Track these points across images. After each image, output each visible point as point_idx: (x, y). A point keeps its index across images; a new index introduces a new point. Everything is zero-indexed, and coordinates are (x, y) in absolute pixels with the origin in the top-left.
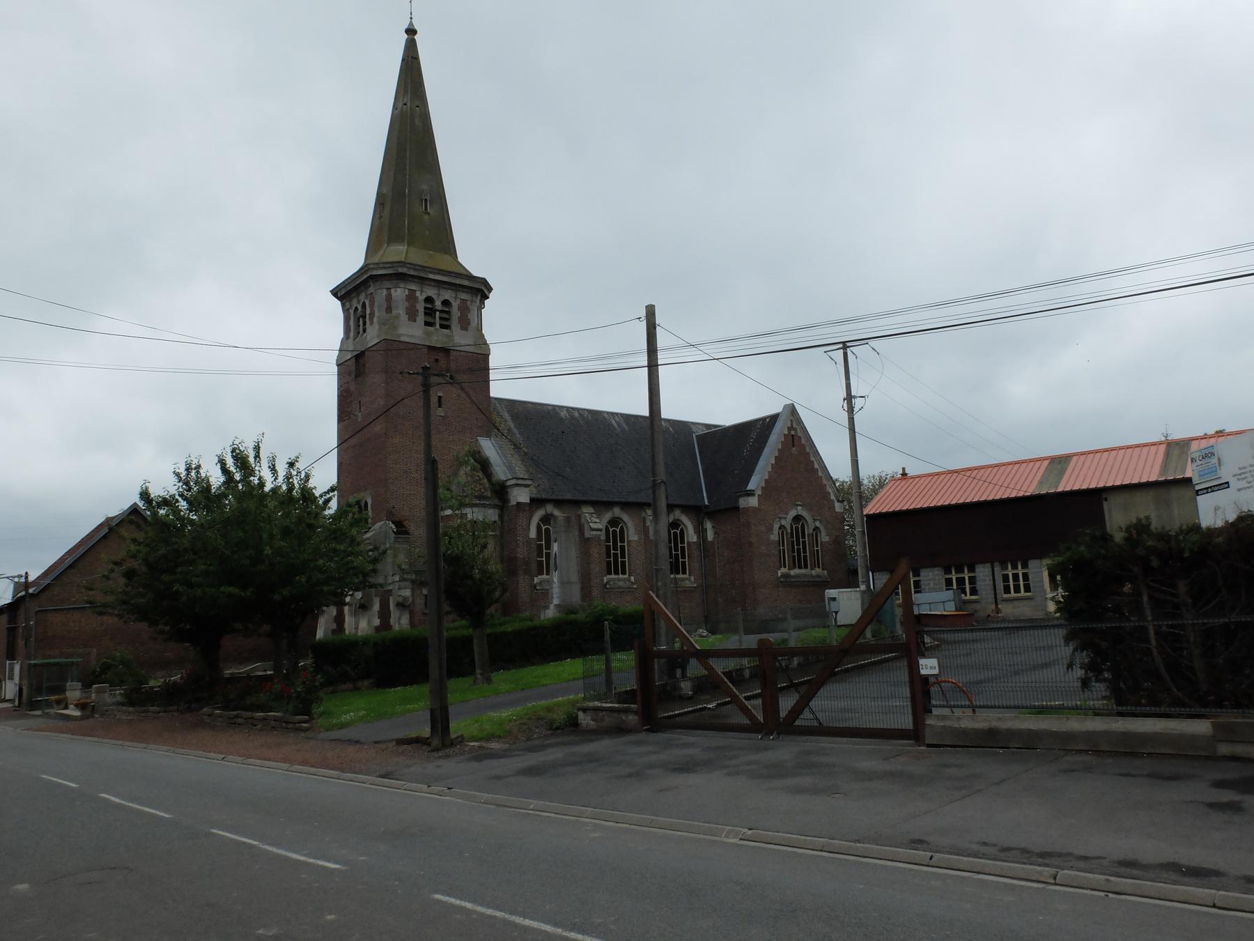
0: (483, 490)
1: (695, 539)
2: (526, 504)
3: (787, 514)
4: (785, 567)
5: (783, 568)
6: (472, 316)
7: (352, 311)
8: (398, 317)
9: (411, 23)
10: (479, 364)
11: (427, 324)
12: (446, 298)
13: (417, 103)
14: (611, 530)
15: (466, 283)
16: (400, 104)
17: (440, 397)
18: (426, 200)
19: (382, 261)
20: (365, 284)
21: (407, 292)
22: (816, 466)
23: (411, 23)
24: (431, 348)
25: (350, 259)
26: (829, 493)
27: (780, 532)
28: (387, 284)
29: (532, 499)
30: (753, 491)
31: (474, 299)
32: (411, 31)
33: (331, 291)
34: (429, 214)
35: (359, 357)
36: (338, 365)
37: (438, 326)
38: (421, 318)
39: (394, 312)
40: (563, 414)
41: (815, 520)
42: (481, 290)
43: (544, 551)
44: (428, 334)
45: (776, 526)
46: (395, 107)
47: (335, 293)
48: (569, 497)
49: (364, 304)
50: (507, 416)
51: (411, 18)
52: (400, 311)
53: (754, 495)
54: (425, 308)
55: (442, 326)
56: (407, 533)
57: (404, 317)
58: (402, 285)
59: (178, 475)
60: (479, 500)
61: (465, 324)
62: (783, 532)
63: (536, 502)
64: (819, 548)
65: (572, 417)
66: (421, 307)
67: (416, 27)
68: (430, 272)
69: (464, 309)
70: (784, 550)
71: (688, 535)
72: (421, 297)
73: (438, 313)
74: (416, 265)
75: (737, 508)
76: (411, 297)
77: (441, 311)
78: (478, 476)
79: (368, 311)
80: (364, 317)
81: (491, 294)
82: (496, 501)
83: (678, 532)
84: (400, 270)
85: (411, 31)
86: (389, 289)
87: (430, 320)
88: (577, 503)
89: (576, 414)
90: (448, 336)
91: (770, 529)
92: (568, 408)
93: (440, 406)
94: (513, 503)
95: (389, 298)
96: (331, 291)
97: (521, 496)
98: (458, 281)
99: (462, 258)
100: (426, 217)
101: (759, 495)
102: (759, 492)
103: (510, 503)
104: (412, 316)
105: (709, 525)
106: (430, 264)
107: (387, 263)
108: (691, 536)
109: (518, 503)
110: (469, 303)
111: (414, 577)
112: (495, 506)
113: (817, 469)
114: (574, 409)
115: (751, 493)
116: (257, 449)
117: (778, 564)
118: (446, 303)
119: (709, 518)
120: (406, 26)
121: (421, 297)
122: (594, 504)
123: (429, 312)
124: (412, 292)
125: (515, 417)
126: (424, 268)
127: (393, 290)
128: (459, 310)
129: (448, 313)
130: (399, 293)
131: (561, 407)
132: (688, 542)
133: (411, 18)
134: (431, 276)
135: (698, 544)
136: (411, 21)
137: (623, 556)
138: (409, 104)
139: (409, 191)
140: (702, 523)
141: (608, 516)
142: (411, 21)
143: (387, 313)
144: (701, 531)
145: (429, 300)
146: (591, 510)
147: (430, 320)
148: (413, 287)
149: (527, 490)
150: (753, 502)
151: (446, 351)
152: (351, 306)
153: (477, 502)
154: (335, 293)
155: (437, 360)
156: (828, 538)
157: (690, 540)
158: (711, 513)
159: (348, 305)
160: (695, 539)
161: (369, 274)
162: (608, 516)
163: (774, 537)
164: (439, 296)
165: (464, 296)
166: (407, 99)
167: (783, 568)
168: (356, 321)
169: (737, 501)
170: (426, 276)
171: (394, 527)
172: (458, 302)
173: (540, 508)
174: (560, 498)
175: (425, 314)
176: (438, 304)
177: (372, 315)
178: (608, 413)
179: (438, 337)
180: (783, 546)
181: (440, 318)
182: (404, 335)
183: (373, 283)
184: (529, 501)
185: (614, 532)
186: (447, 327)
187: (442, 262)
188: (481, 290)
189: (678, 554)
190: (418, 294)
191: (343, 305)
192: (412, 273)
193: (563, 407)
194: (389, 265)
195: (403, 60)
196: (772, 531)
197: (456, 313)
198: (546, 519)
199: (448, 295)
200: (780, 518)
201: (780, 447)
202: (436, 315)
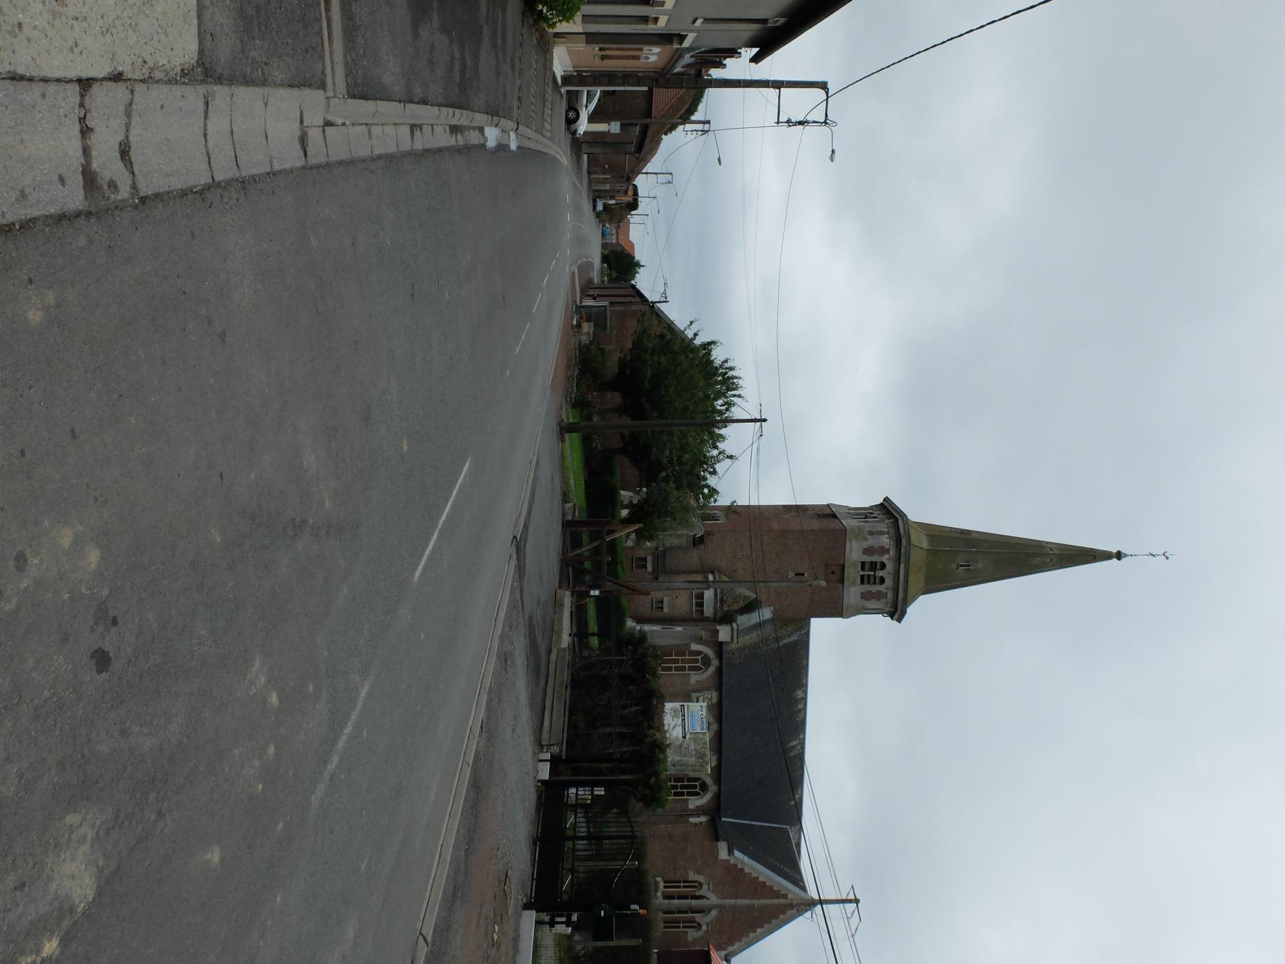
0: (728, 603)
1: (691, 806)
2: (718, 638)
3: (712, 891)
4: (665, 887)
5: (663, 925)
6: (872, 604)
7: (871, 511)
8: (865, 539)
9: (1126, 555)
10: (836, 609)
11: (863, 564)
12: (886, 581)
13: (1054, 560)
14: (697, 783)
15: (901, 596)
16: (1051, 546)
17: (803, 575)
18: (969, 566)
19: (910, 528)
20: (893, 516)
21: (887, 547)
22: (759, 930)
23: (1126, 555)
24: (843, 566)
25: (917, 511)
26: (733, 945)
27: (696, 884)
28: (892, 531)
29: (721, 642)
30: (733, 854)
31: (889, 605)
32: (1119, 556)
33: (887, 497)
34: (958, 568)
35: (834, 516)
36: (828, 505)
37: (862, 573)
38: (868, 559)
39: (869, 537)
40: (799, 693)
41: (708, 924)
42: (896, 612)
43: (679, 784)
44: (854, 564)
45: (701, 878)
46: (1048, 543)
47: (886, 499)
48: (725, 680)
49: (876, 518)
50: (794, 638)
51: (1131, 555)
52: (871, 541)
53: (729, 855)
54: (876, 562)
55: (862, 577)
56: (694, 546)
57: (866, 545)
58: (892, 543)
59: (726, 361)
60: (721, 600)
61: (866, 596)
62: (695, 887)
63: (719, 647)
64: (682, 929)
65: (797, 701)
66: (876, 558)
67: (1123, 560)
68: (905, 565)
69: (880, 596)
70: (679, 927)
71: (693, 799)
72: (885, 558)
73: (872, 573)
74: (909, 552)
75: (717, 839)
76: (883, 551)
77: (875, 577)
78: (740, 602)
79: (869, 520)
80: (866, 517)
81: (895, 622)
82: (719, 615)
83: (697, 790)
84: (904, 540)
85: (1119, 556)
86: (888, 533)
87: (867, 566)
88: (719, 689)
89: (800, 706)
90: (854, 583)
91: (698, 871)
92: (805, 699)
93: (796, 574)
94: (718, 627)
95: (881, 533)
96: (887, 497)
97: (724, 633)
98: (901, 589)
99: (923, 599)
100: (954, 566)
101: (729, 860)
102: (732, 861)
103: (719, 625)
104: (868, 551)
105: (703, 819)
106: (912, 568)
107: (908, 530)
108: (695, 802)
109: (718, 631)
110: (884, 600)
111: (661, 549)
112: (715, 612)
113: (755, 932)
114: (805, 705)
115: (730, 852)
116: (739, 396)
117: (667, 879)
118: (882, 580)
119: (709, 820)
120: (1123, 551)
121: (885, 558)
122: (720, 703)
123: (873, 566)
124: (887, 551)
125: (796, 643)
126: (908, 559)
127: (887, 536)
128: (878, 591)
129: (875, 583)
130: (885, 541)
131: (806, 692)
132: (688, 799)
133: (1131, 555)
134: (902, 566)
135: (686, 809)
136: (1128, 555)
137: (677, 669)
138: (1051, 552)
139: (974, 551)
140: (704, 814)
141: (709, 781)
142: (1128, 555)
143: (868, 532)
144: (699, 811)
145: (883, 566)
146: (715, 701)
147: (867, 566)
148: (891, 553)
149: (729, 640)
150: (723, 854)
151: (842, 581)
152: (876, 511)
153: (719, 598)
154: (886, 499)
155: (833, 573)
156: (691, 940)
157: (690, 802)
158: (713, 822)
159: (875, 509)
160: (691, 806)
161: (899, 518)
162: (709, 781)
163: (692, 876)
164: (886, 573)
165: (890, 595)
166: (1056, 551)
167: (663, 925)
168: (864, 514)
169: (725, 840)
170: (901, 562)
171: (699, 535)
172: (885, 591)
173: (716, 654)
174: (724, 671)
175: (872, 562)
176: (880, 573)
177: (867, 522)
178: (804, 739)
179: (853, 573)
180: (684, 887)
181: (869, 576)
182: (851, 544)
183: (892, 522)
184: (720, 640)
185: (695, 787)
186: (862, 582)
187: (917, 579)
188: (896, 612)
189: (677, 789)
190: (887, 556)
191: (876, 506)
192: (903, 550)
193: (806, 694)
194: (907, 531)
195: (1092, 549)
196: (697, 873)
197: (875, 588)
198: (706, 661)
199: (889, 581)
200: (709, 884)
201: (775, 888)
202: (870, 572)
